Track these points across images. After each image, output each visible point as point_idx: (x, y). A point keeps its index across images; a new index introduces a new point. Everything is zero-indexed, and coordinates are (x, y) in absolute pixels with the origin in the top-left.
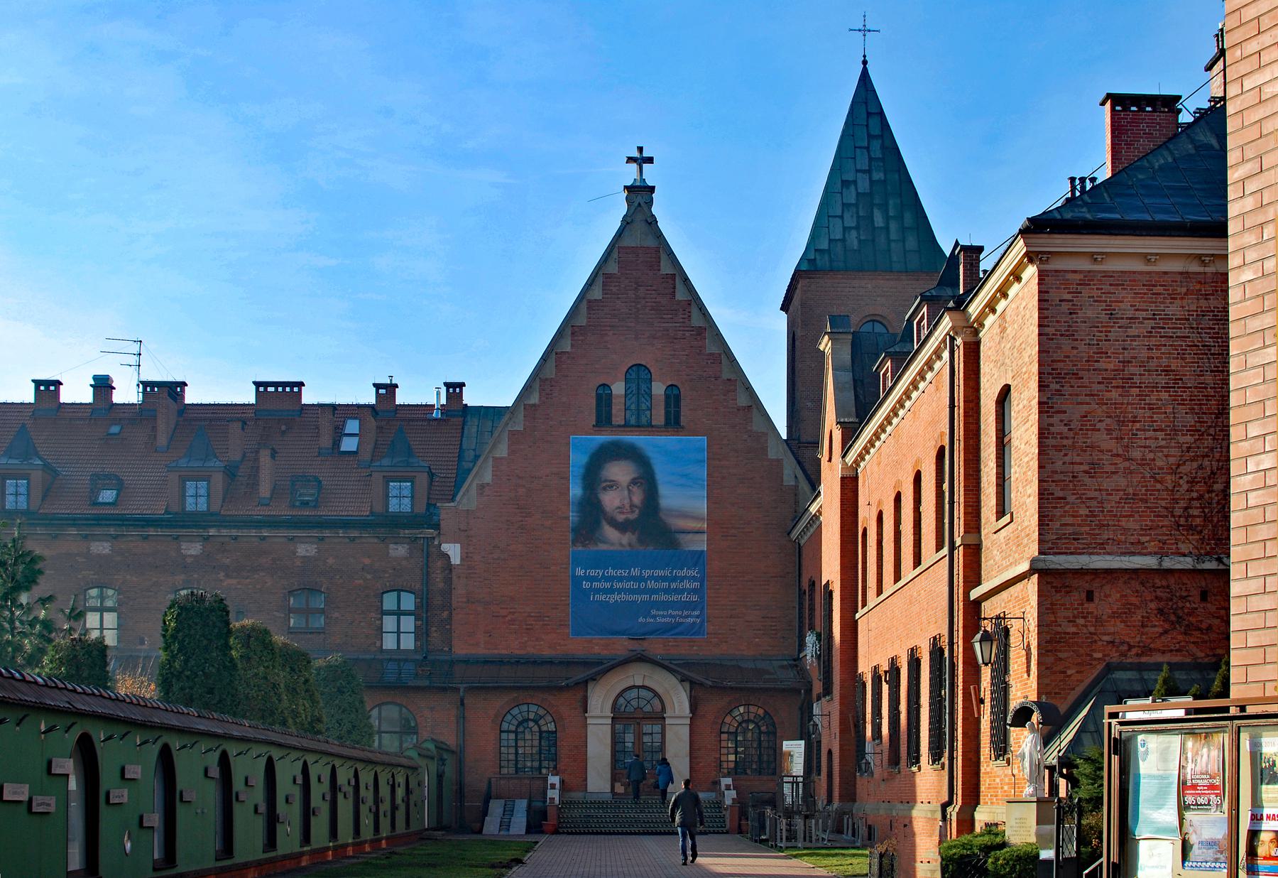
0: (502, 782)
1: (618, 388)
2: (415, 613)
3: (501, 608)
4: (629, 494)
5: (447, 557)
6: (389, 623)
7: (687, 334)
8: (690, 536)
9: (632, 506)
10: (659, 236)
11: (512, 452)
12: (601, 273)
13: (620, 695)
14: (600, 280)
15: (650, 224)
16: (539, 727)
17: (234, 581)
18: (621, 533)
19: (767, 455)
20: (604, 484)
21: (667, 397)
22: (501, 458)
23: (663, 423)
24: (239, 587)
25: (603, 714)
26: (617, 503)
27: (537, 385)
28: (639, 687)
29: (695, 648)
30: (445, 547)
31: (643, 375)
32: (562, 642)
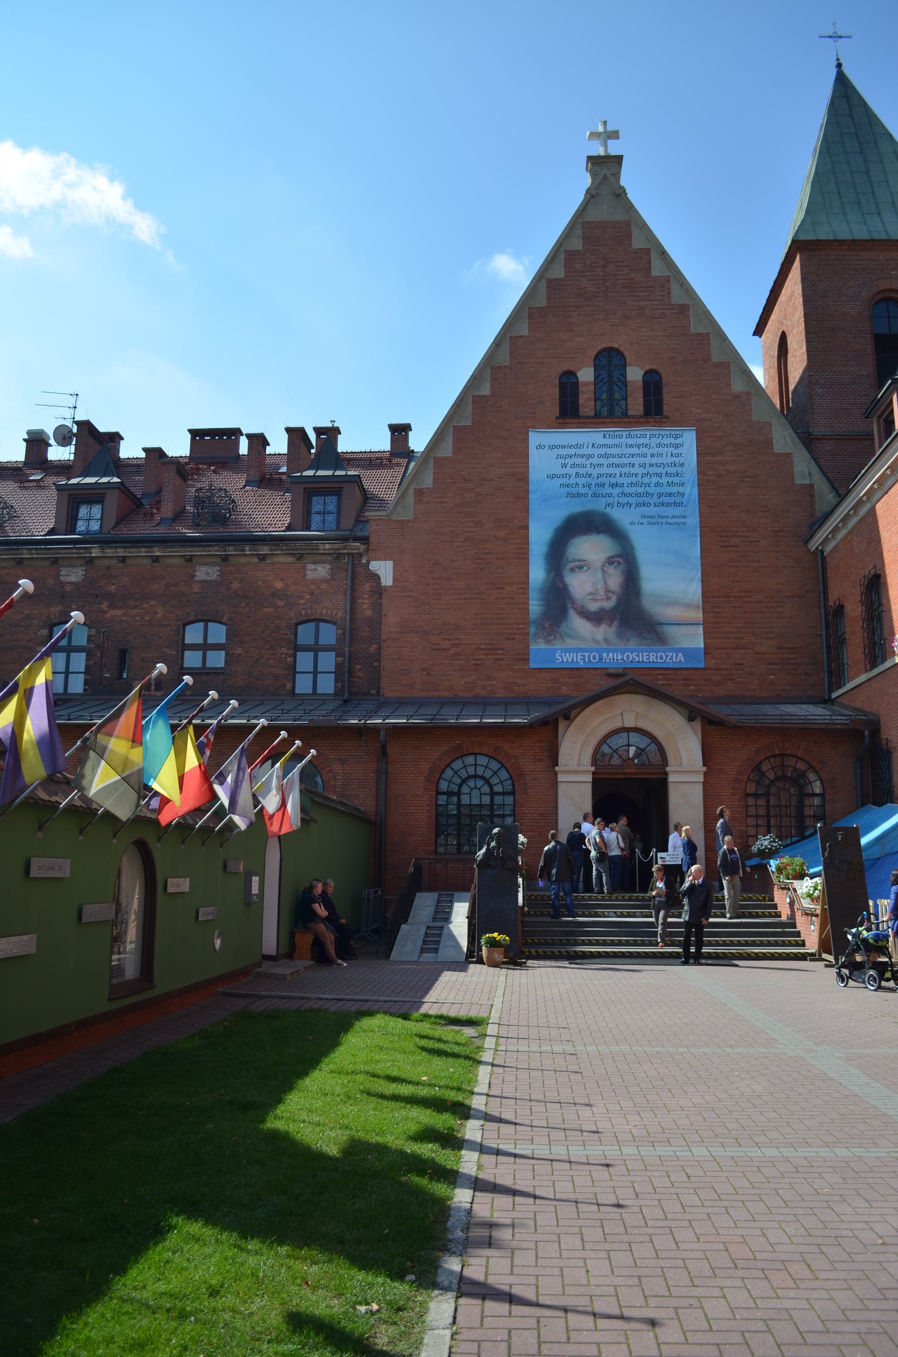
0: (439, 866)
1: (586, 375)
2: (337, 650)
3: (443, 639)
4: (604, 576)
5: (376, 577)
6: (304, 661)
7: (667, 312)
8: (684, 629)
9: (607, 591)
11: (457, 450)
12: (562, 250)
13: (604, 740)
14: (562, 257)
15: (619, 195)
17: (119, 612)
18: (595, 626)
19: (772, 448)
20: (572, 565)
21: (646, 384)
22: (444, 459)
23: (642, 413)
24: (124, 618)
25: (581, 768)
26: (588, 588)
27: (488, 374)
28: (628, 730)
29: (691, 688)
30: (375, 566)
32: (520, 681)
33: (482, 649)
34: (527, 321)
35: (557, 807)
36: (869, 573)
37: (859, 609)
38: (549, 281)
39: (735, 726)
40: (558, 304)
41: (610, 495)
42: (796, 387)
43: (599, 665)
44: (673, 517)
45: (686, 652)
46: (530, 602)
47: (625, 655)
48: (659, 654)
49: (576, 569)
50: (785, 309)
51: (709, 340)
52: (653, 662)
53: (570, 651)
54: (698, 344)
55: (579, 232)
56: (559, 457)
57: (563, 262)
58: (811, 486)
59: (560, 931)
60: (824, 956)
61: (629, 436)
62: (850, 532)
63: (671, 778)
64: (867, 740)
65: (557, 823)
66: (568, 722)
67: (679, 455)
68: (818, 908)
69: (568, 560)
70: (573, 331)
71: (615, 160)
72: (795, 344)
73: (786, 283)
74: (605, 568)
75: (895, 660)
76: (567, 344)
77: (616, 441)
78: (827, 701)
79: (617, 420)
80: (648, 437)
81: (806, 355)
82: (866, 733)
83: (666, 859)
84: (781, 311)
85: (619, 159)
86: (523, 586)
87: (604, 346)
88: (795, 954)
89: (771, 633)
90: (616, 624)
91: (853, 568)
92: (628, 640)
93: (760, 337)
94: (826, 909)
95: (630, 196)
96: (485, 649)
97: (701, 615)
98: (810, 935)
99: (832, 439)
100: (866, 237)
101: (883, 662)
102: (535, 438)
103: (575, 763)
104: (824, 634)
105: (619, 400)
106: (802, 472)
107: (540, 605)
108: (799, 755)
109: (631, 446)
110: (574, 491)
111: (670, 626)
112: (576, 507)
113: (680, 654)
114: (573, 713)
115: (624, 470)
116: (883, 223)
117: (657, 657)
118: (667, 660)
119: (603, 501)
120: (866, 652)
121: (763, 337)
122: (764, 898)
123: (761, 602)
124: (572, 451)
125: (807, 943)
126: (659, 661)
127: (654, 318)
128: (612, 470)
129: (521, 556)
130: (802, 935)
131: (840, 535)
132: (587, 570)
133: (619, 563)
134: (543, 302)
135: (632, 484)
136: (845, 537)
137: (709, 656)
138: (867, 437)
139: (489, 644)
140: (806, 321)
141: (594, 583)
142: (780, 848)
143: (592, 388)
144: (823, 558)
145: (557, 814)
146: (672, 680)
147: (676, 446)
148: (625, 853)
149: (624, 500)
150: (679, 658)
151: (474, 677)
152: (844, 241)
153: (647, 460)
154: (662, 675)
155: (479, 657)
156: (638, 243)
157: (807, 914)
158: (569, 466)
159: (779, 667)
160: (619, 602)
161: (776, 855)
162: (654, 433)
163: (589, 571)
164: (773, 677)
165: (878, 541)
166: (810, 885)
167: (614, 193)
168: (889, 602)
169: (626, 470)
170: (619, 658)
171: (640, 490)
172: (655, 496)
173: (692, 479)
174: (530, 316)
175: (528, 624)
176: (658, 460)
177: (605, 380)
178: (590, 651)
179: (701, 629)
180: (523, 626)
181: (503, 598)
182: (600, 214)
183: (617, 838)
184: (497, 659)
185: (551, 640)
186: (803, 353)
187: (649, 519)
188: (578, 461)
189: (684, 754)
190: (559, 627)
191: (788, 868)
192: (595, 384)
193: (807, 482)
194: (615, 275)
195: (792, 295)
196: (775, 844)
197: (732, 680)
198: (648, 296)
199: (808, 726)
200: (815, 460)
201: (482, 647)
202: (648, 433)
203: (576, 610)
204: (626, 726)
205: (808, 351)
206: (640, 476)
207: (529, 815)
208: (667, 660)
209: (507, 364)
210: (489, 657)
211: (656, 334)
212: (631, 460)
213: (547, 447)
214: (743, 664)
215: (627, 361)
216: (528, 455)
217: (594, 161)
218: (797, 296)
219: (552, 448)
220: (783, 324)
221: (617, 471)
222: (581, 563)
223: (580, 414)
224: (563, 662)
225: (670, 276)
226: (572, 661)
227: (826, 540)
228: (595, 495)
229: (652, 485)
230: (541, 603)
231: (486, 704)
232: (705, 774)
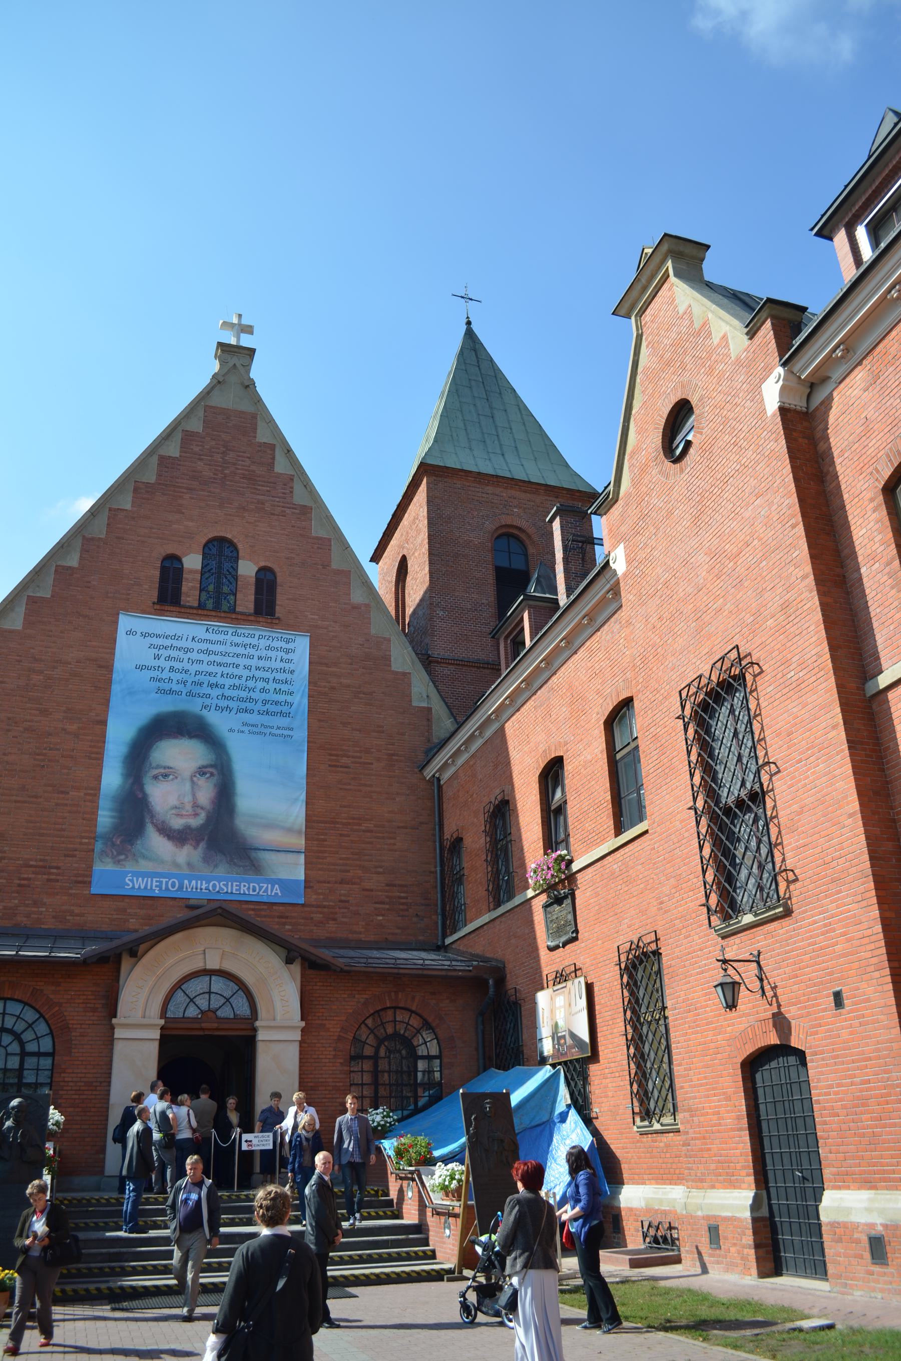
1: (193, 562)
4: (193, 788)
7: (288, 511)
8: (282, 857)
9: (195, 805)
10: (258, 401)
11: (28, 622)
12: (180, 429)
15: (247, 387)
16: (22, 1044)
19: (390, 665)
20: (155, 772)
21: (259, 582)
23: (252, 611)
26: (173, 801)
27: (78, 543)
29: (287, 927)
31: (227, 552)
32: (77, 910)
33: (31, 866)
34: (131, 495)
35: (110, 1073)
36: (496, 798)
37: (482, 841)
38: (162, 458)
39: (342, 971)
40: (168, 483)
41: (208, 696)
42: (415, 610)
43: (179, 895)
44: (279, 728)
45: (282, 883)
46: (99, 812)
47: (211, 884)
48: (251, 885)
49: (160, 777)
50: (407, 533)
51: (331, 545)
52: (244, 894)
53: (144, 875)
54: (318, 548)
55: (201, 414)
56: (151, 646)
57: (179, 441)
58: (429, 710)
59: (101, 1254)
60: (467, 1273)
61: (235, 634)
62: (473, 756)
63: (261, 1036)
64: (491, 990)
65: (109, 1095)
66: (134, 960)
67: (290, 661)
68: (457, 1206)
69: (151, 764)
70: (183, 513)
71: (246, 352)
72: (416, 567)
73: (410, 507)
74: (195, 779)
75: (526, 895)
76: (175, 526)
77: (221, 637)
78: (440, 948)
79: (223, 615)
80: (257, 637)
81: (428, 576)
82: (491, 982)
83: (254, 1142)
84: (402, 535)
85: (251, 352)
86: (92, 792)
87: (216, 534)
88: (427, 1272)
89: (381, 867)
90: (202, 845)
91: (475, 796)
92: (216, 866)
93: (377, 564)
94: (472, 1206)
95: (260, 389)
96: (35, 867)
97: (303, 842)
98: (444, 1243)
99: (453, 664)
100: (491, 472)
101: (510, 897)
102: (125, 622)
103: (140, 1013)
104: (438, 871)
105: (228, 594)
106: (421, 694)
107: (112, 817)
108: (414, 1008)
109: (237, 645)
110: (167, 686)
111: (266, 852)
112: (167, 705)
113: (277, 886)
114: (142, 948)
115: (226, 670)
116: (507, 463)
117: (249, 888)
118: (261, 893)
119: (199, 701)
120: (490, 888)
121: (380, 563)
122: (377, 1192)
123: (371, 831)
124: (168, 642)
125: (437, 1254)
126: (251, 893)
127: (273, 514)
128: (212, 669)
129: (93, 755)
130: (431, 1243)
131: (461, 761)
132: (172, 780)
133: (212, 774)
134: (152, 478)
135: (234, 687)
136: (467, 762)
137: (309, 890)
138: (486, 666)
139: (41, 860)
140: (429, 543)
141: (179, 796)
142: (394, 1124)
143: (198, 576)
144: (440, 787)
145: (110, 1082)
146: (265, 916)
147: (288, 651)
148: (197, 1135)
149: (223, 703)
150: (274, 891)
151: (16, 901)
152: (471, 472)
153: (254, 662)
154: (253, 910)
155: (26, 876)
156: (263, 436)
157: (438, 1214)
158: (162, 659)
159: (387, 906)
160: (209, 819)
161: (389, 1134)
162: (264, 634)
163: (176, 781)
164: (381, 918)
165: (508, 763)
166: (446, 1173)
167: (242, 384)
168: (519, 830)
169: (230, 670)
170: (203, 887)
171: (243, 694)
172: (260, 703)
173: (303, 688)
174: (136, 490)
175: (94, 838)
176: (267, 664)
177: (214, 571)
178: (169, 876)
179: (302, 858)
180: (87, 841)
181: (66, 805)
182: (224, 400)
183: (188, 1115)
184: (49, 880)
185: (122, 860)
186: (425, 575)
187: (250, 728)
188: (174, 653)
189: (278, 1005)
190: (132, 845)
191: (411, 1150)
192: (202, 573)
193: (424, 705)
194: (234, 464)
195: (416, 518)
196: (389, 1120)
197: (334, 919)
198: (268, 491)
199: (425, 972)
200: (434, 684)
201: (32, 863)
202: (257, 633)
203: (155, 826)
204: (208, 967)
205: (431, 572)
206: (244, 679)
207: (71, 1084)
208: (261, 893)
209: (103, 536)
210: (40, 876)
211: (274, 531)
212: (235, 660)
213: (139, 634)
214: (347, 901)
215: (240, 554)
216: (115, 641)
217: (223, 347)
218: (422, 518)
219: (144, 635)
220: (403, 548)
221: (219, 670)
222: (167, 771)
223: (182, 603)
224: (133, 887)
225: (294, 476)
226: (146, 887)
227: (445, 766)
228: (190, 694)
229: (257, 690)
230: (114, 814)
231: (28, 937)
232: (303, 1031)
